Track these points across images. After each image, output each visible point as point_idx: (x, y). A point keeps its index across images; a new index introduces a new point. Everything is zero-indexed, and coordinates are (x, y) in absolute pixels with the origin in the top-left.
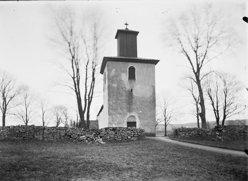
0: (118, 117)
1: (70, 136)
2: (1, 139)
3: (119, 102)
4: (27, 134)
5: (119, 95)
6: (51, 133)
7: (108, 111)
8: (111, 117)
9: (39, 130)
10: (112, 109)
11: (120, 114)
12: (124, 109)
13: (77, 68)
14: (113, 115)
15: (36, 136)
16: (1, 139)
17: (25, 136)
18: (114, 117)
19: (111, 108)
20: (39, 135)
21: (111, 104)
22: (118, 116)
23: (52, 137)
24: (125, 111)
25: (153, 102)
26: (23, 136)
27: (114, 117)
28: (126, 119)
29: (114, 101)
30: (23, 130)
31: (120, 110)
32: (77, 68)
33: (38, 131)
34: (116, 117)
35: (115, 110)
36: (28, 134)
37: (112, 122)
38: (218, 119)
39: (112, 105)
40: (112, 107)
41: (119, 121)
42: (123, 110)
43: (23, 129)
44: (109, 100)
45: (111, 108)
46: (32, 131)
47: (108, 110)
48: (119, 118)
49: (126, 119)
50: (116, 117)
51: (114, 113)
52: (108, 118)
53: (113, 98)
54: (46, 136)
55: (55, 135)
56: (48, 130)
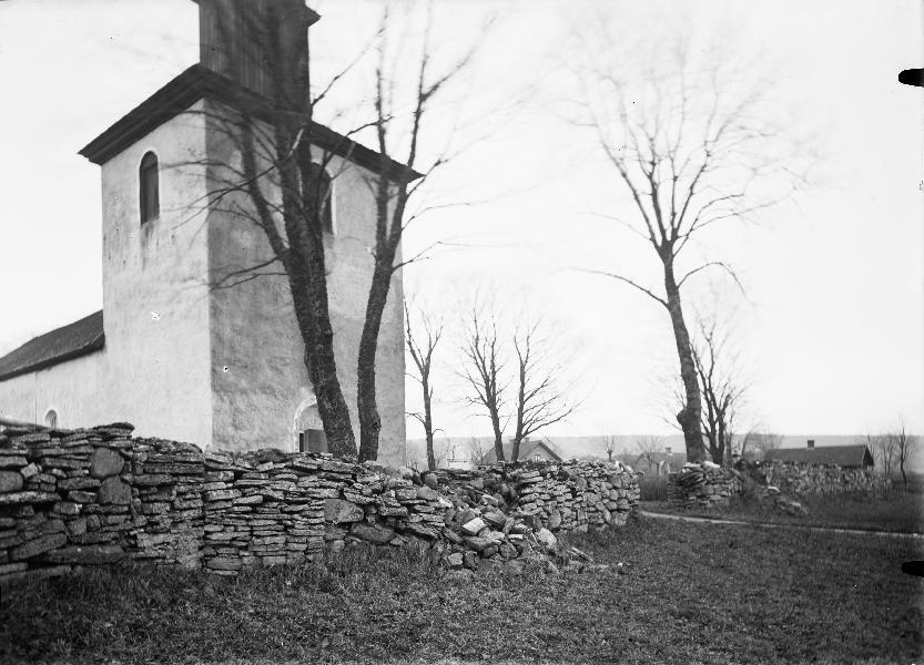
0: (260, 406)
1: (398, 525)
2: (3, 578)
3: (265, 328)
4: (68, 519)
5: (263, 292)
6: (268, 499)
7: (213, 370)
8: (226, 406)
9: (167, 479)
10: (231, 363)
11: (267, 389)
12: (287, 371)
13: (676, 226)
14: (238, 397)
15: (146, 541)
16: (3, 578)
17: (51, 544)
18: (241, 403)
19: (226, 354)
20: (175, 524)
21: (227, 333)
22: (260, 400)
23: (280, 539)
24: (290, 377)
25: (395, 351)
26: (34, 549)
27: (241, 403)
28: (296, 417)
29: (238, 322)
30: (27, 484)
31: (269, 373)
32: (676, 226)
33: (163, 487)
34: (250, 405)
35: (248, 368)
36: (79, 527)
37: (230, 430)
38: (498, 434)
39: (231, 341)
40: (233, 349)
41: (265, 427)
42: (281, 372)
43: (31, 470)
44: (215, 312)
45: (226, 354)
46: (116, 492)
47: (213, 364)
48: (266, 413)
49: (296, 417)
50: (250, 405)
51: (244, 383)
52: (210, 411)
53: (237, 303)
54: (228, 536)
55: (300, 522)
56: (238, 475)
